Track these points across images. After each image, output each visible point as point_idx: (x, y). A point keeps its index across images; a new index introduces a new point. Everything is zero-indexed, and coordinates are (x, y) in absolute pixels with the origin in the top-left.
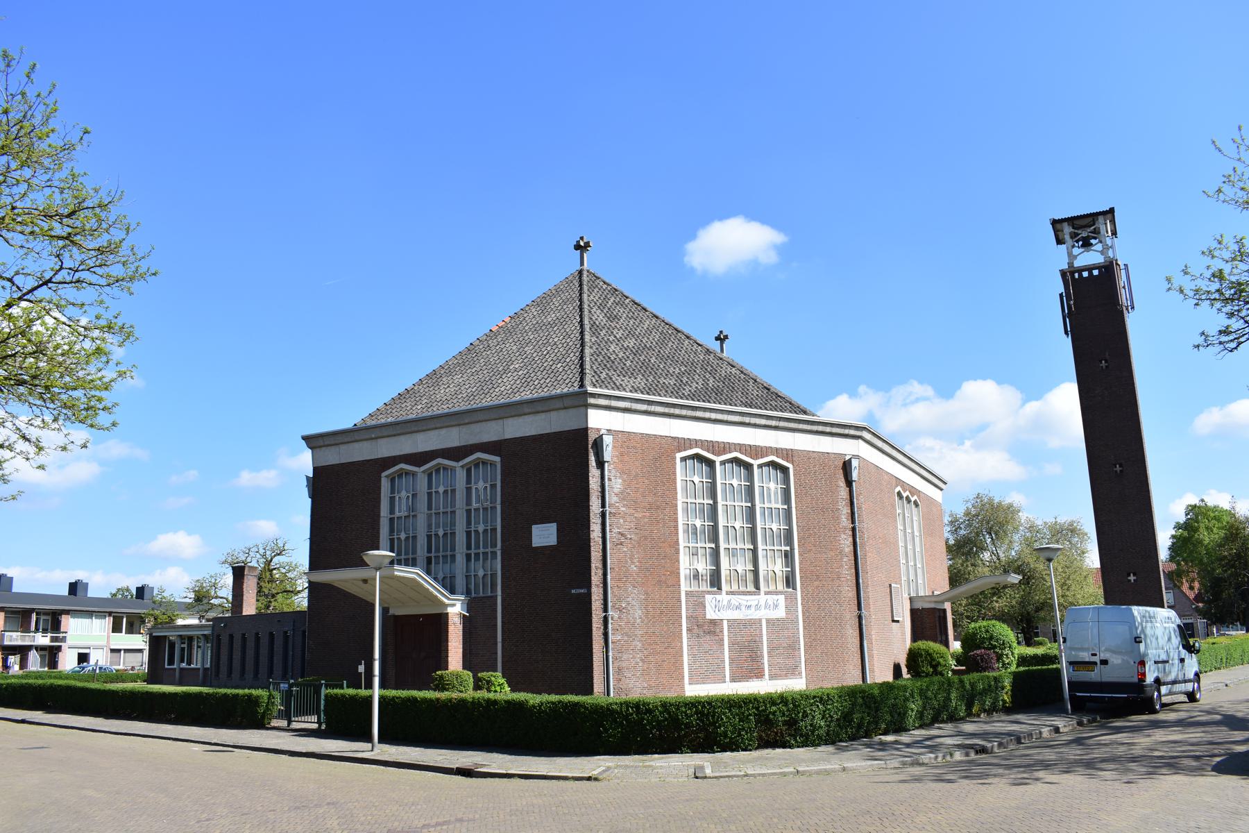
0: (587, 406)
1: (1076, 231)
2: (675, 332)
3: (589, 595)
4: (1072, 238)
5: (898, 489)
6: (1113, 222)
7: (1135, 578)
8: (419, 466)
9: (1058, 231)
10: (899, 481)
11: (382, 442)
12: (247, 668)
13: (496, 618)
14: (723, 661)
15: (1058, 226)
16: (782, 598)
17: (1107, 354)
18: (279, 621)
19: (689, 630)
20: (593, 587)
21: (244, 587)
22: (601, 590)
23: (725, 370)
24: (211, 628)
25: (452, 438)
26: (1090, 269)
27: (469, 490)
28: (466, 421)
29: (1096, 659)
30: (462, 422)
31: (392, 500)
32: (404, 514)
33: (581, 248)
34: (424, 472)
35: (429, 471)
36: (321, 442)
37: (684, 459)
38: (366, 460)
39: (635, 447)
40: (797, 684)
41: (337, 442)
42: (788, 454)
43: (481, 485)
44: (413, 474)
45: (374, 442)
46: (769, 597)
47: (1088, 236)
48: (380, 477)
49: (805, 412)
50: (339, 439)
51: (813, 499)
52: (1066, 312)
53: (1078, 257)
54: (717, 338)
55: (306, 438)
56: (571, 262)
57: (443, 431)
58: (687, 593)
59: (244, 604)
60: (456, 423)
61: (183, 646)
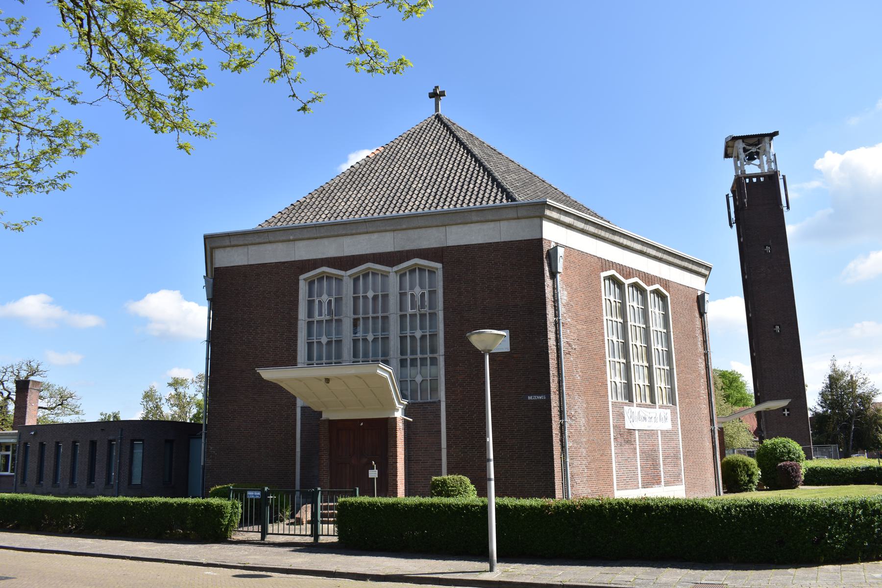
0: (543, 217)
3: (548, 401)
8: (346, 270)
11: (300, 244)
12: (45, 472)
13: (440, 424)
16: (668, 411)
17: (770, 241)
18: (102, 430)
20: (552, 393)
21: (28, 399)
24: (16, 437)
25: (386, 243)
27: (402, 295)
28: (404, 227)
30: (399, 227)
31: (310, 303)
32: (325, 317)
33: (436, 95)
34: (350, 276)
35: (356, 276)
38: (280, 262)
41: (246, 242)
43: (418, 291)
45: (291, 244)
46: (661, 410)
48: (298, 280)
50: (250, 239)
56: (427, 109)
57: (376, 236)
59: (27, 415)
60: (392, 228)
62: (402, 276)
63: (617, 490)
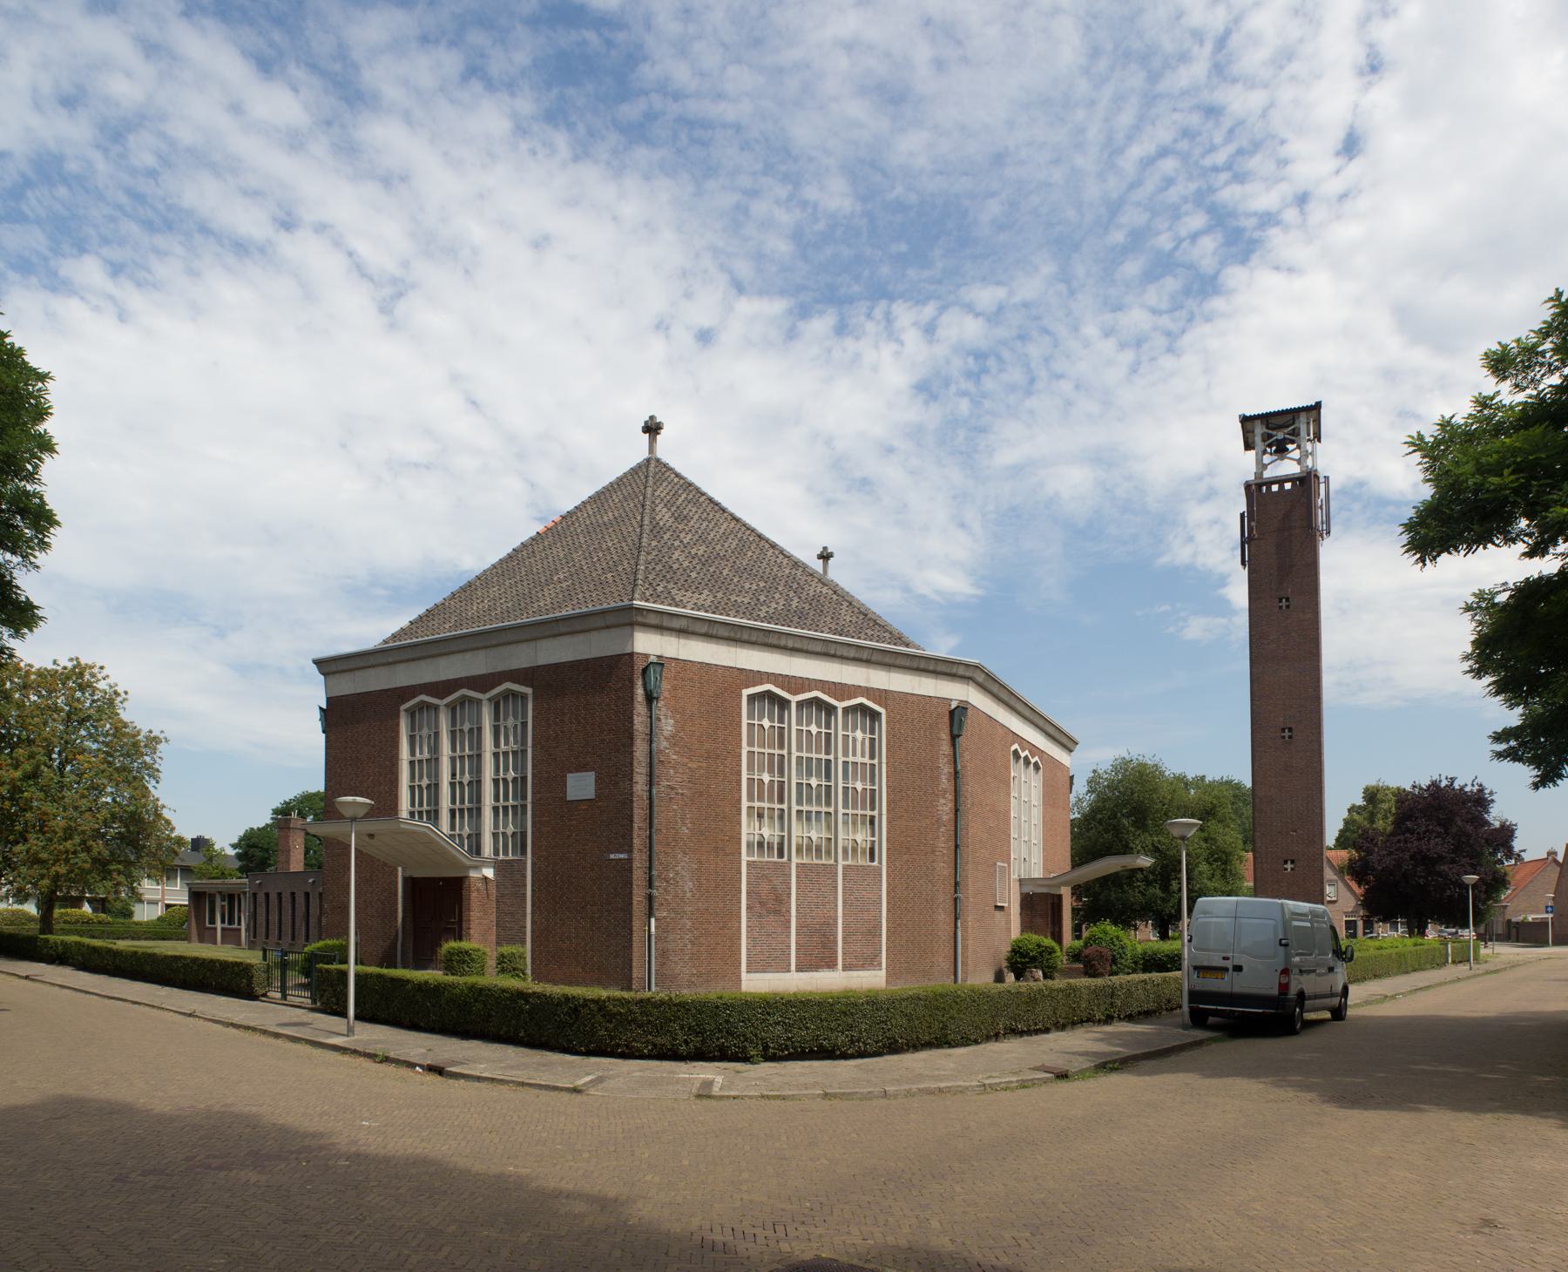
1: (1270, 432)
2: (757, 539)
4: (1264, 441)
5: (1015, 746)
6: (1318, 421)
7: (1292, 866)
8: (442, 698)
9: (1248, 432)
10: (1017, 738)
14: (789, 947)
15: (1249, 425)
19: (749, 908)
20: (635, 851)
22: (645, 857)
23: (814, 588)
26: (1281, 481)
28: (494, 642)
29: (1229, 964)
36: (333, 668)
37: (752, 698)
39: (691, 680)
40: (873, 979)
42: (881, 696)
43: (511, 722)
44: (435, 708)
47: (1285, 438)
48: (399, 711)
49: (907, 645)
51: (908, 753)
52: (1246, 535)
53: (1269, 467)
54: (821, 557)
55: (319, 663)
58: (749, 864)
61: (223, 903)
62: (454, 711)
63: (748, 972)
